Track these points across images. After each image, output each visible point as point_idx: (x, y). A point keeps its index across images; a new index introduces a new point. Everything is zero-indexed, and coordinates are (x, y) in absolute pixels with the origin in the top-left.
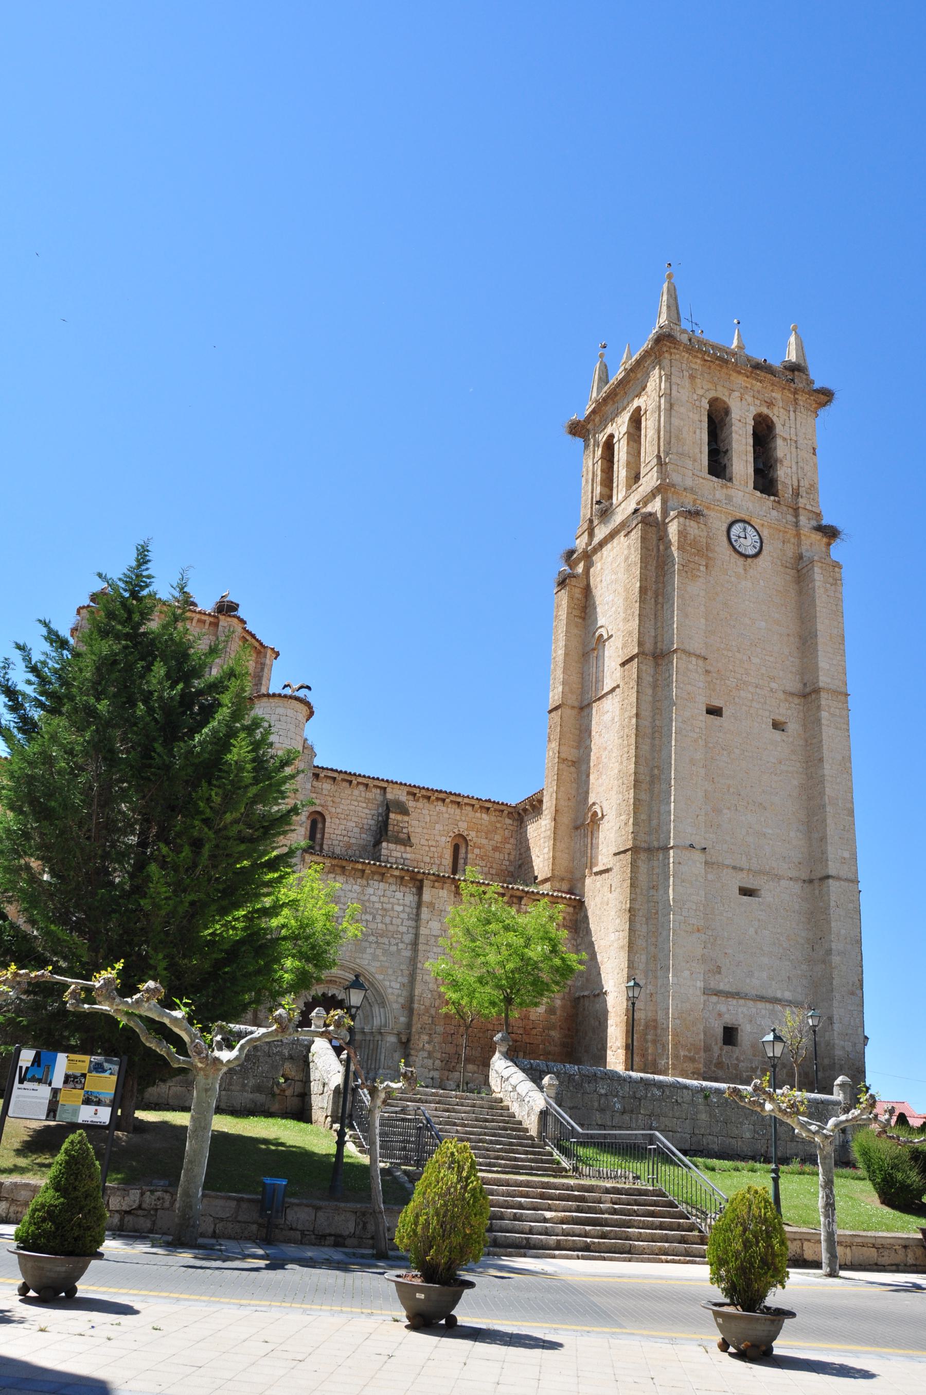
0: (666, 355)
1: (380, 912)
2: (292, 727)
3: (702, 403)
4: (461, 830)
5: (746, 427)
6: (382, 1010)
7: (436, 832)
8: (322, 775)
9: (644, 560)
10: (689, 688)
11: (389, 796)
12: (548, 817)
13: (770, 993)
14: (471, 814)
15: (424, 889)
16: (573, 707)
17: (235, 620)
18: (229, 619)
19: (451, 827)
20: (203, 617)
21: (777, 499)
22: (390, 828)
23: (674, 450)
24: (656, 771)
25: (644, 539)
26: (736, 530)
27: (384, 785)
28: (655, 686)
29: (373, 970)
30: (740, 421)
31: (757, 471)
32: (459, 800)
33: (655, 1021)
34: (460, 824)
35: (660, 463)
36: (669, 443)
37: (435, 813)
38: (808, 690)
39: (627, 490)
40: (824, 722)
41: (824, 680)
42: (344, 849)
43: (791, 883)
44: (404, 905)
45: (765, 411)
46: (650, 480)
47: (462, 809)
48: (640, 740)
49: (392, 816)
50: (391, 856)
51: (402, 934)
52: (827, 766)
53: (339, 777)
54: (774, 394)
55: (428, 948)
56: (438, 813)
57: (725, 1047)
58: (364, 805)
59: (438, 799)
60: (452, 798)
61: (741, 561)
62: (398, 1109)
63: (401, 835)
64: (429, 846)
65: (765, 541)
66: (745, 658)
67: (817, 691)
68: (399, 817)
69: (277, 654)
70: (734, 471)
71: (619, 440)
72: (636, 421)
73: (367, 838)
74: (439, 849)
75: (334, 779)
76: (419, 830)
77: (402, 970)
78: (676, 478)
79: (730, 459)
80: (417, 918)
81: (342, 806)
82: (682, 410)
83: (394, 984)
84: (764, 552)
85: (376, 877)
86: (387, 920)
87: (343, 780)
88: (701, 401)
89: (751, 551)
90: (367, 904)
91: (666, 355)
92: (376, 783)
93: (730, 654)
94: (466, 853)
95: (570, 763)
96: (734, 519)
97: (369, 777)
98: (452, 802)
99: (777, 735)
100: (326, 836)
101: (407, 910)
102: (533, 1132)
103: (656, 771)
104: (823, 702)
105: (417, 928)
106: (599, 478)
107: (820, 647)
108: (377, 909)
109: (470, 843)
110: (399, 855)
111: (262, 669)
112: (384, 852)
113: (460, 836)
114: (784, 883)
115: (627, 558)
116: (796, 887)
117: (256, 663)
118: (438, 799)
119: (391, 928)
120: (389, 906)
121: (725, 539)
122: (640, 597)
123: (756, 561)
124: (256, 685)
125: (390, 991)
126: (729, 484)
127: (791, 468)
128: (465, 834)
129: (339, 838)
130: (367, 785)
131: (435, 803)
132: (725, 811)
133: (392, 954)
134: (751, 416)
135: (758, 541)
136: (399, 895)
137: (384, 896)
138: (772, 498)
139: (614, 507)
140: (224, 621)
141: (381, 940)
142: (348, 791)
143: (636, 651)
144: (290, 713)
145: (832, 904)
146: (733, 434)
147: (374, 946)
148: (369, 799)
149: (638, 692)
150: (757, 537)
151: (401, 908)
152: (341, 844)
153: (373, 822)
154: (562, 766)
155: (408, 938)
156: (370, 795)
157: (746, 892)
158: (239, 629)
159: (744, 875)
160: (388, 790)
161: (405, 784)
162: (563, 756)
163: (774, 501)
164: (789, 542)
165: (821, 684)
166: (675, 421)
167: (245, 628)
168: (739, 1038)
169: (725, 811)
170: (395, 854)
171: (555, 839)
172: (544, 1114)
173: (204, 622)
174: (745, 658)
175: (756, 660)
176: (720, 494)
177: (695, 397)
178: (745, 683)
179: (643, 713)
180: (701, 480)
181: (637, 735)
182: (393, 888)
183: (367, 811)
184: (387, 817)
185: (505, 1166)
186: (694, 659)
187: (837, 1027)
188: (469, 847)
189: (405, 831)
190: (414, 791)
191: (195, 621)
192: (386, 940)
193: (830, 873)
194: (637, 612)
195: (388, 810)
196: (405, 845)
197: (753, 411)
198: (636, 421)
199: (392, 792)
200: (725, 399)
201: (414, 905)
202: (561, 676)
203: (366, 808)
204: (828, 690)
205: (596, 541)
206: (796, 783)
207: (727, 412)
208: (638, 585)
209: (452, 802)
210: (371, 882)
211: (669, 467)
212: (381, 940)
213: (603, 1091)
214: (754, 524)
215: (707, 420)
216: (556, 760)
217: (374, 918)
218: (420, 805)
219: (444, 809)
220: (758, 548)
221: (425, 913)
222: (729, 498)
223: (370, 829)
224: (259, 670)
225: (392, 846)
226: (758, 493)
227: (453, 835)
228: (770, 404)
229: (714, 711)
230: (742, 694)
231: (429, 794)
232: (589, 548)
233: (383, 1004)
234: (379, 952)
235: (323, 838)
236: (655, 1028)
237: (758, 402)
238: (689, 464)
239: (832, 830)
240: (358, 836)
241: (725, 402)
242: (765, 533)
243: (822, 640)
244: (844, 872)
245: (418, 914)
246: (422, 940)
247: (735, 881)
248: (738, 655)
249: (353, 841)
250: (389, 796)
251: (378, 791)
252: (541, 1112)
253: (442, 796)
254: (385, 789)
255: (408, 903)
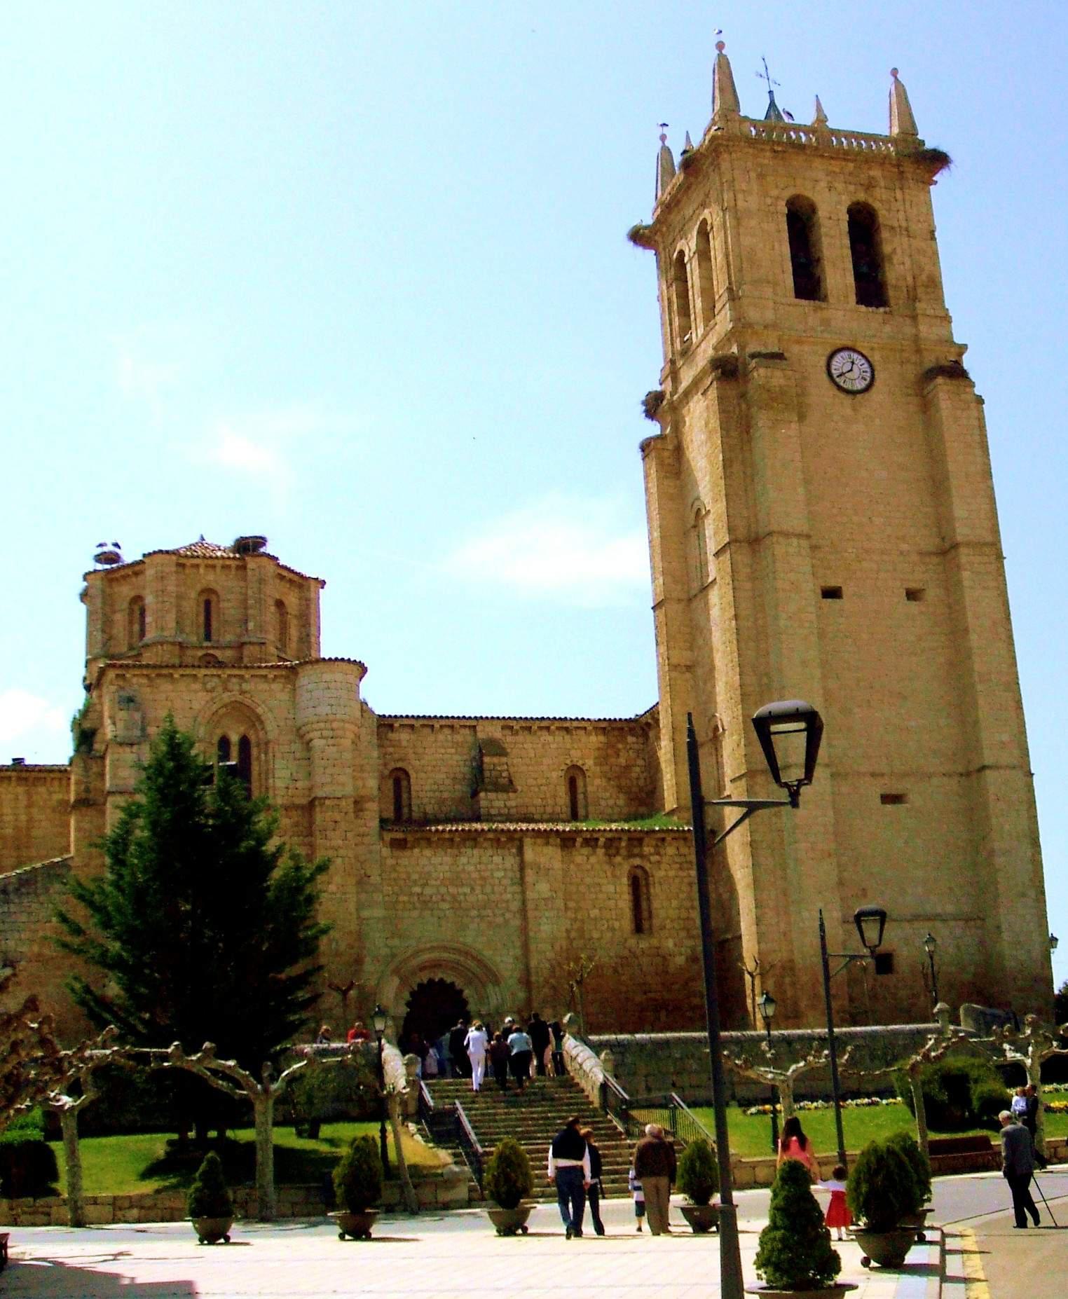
0: (726, 156)
1: (479, 882)
2: (343, 693)
3: (779, 208)
4: (575, 760)
5: (838, 225)
6: (497, 989)
7: (545, 768)
8: (396, 725)
9: (725, 428)
10: (792, 576)
11: (481, 735)
12: (667, 737)
13: (928, 909)
14: (584, 739)
15: (525, 848)
16: (679, 600)
17: (265, 559)
18: (258, 560)
19: (562, 758)
20: (228, 562)
21: (888, 309)
22: (487, 774)
23: (747, 278)
24: (765, 680)
25: (721, 399)
26: (839, 362)
27: (473, 723)
28: (753, 578)
29: (479, 946)
30: (830, 218)
31: (858, 276)
32: (567, 724)
33: (791, 961)
34: (573, 752)
35: (733, 297)
36: (741, 270)
37: (540, 746)
38: (947, 545)
39: (706, 326)
40: (966, 583)
41: (962, 532)
42: (436, 807)
43: (945, 779)
44: (505, 870)
45: (861, 196)
46: (724, 322)
47: (572, 735)
48: (743, 645)
49: (486, 759)
50: (492, 807)
51: (507, 901)
52: (973, 637)
53: (417, 724)
54: (872, 173)
55: (537, 913)
56: (544, 745)
57: (879, 977)
58: (453, 751)
59: (540, 728)
60: (557, 724)
61: (847, 400)
62: (468, 1100)
63: (502, 781)
64: (539, 786)
65: (877, 368)
66: (865, 520)
67: (955, 546)
68: (495, 760)
69: (323, 583)
70: (829, 286)
71: (690, 259)
72: (704, 234)
73: (462, 789)
74: (552, 787)
75: (412, 727)
76: (524, 768)
77: (513, 942)
78: (753, 315)
79: (823, 270)
80: (522, 881)
81: (426, 757)
82: (753, 223)
83: (504, 959)
84: (877, 383)
85: (468, 843)
86: (488, 889)
87: (423, 726)
88: (776, 206)
89: (860, 385)
90: (462, 876)
91: (726, 156)
92: (463, 722)
93: (845, 519)
94: (585, 786)
95: (684, 669)
96: (834, 348)
97: (453, 717)
98: (558, 728)
99: (914, 607)
100: (413, 793)
101: (510, 874)
102: (597, 1104)
103: (765, 680)
104: (963, 559)
105: (523, 892)
106: (675, 307)
107: (954, 492)
108: (474, 880)
109: (588, 774)
110: (501, 804)
111: (308, 606)
112: (483, 803)
113: (575, 767)
114: (935, 781)
115: (707, 424)
116: (953, 784)
117: (300, 599)
118: (540, 728)
119: (493, 897)
120: (488, 874)
121: (825, 376)
122: (725, 472)
123: (866, 395)
124: (304, 626)
125: (502, 966)
126: (824, 305)
127: (903, 263)
128: (579, 764)
129: (429, 794)
130: (452, 727)
131: (539, 733)
132: (856, 710)
133: (499, 926)
134: (845, 210)
135: (868, 370)
136: (497, 859)
137: (480, 863)
138: (882, 310)
139: (694, 347)
140: (252, 563)
141: (484, 913)
142: (431, 738)
143: (727, 540)
144: (339, 677)
145: (992, 797)
146: (823, 239)
147: (477, 920)
148: (457, 743)
149: (734, 589)
150: (866, 365)
151: (501, 874)
152: (433, 802)
153: (466, 768)
154: (674, 674)
155: (515, 905)
156: (458, 738)
157: (889, 799)
158: (271, 568)
159: (886, 780)
160: (479, 728)
161: (498, 718)
162: (674, 661)
163: (885, 313)
164: (908, 361)
165: (959, 539)
166: (746, 241)
167: (278, 564)
168: (895, 962)
169: (856, 710)
170: (496, 804)
171: (676, 764)
172: (604, 1087)
173: (229, 567)
174: (865, 520)
175: (877, 520)
176: (813, 320)
177: (769, 201)
178: (867, 551)
179: (743, 613)
180: (787, 308)
181: (738, 641)
182: (490, 852)
183: (457, 757)
184: (482, 762)
185: (606, 1135)
186: (795, 541)
187: (1005, 936)
188: (588, 779)
189: (505, 774)
190: (508, 724)
191: (218, 569)
192: (489, 912)
193: (986, 763)
194: (723, 492)
195: (481, 755)
196: (507, 791)
197: (846, 201)
198: (704, 234)
199: (483, 731)
200: (808, 194)
201: (516, 867)
202: (661, 565)
203: (456, 753)
204: (968, 544)
205: (681, 389)
206: (942, 660)
207: (813, 209)
208: (721, 458)
209: (558, 728)
210: (463, 850)
211: (745, 301)
212: (484, 913)
213: (677, 1056)
214: (860, 349)
215: (786, 227)
216: (667, 668)
217: (473, 889)
218: (520, 738)
219: (550, 738)
220: (868, 379)
221: (530, 876)
222: (826, 323)
223: (464, 778)
224: (304, 608)
225: (492, 795)
226: (863, 308)
227: (565, 767)
228: (870, 186)
229: (832, 593)
230: (865, 564)
231: (528, 724)
232: (675, 397)
233: (496, 981)
234: (483, 926)
235: (410, 798)
236: (792, 969)
237: (852, 188)
238: (768, 291)
239: (984, 711)
240: (450, 788)
241: (808, 199)
242: (876, 358)
243: (956, 483)
244: (1006, 758)
245: (522, 878)
246: (530, 905)
247: (875, 790)
248: (855, 519)
249: (446, 795)
250: (481, 735)
251: (467, 731)
252: (601, 1084)
253: (544, 724)
254: (474, 727)
255: (508, 865)
